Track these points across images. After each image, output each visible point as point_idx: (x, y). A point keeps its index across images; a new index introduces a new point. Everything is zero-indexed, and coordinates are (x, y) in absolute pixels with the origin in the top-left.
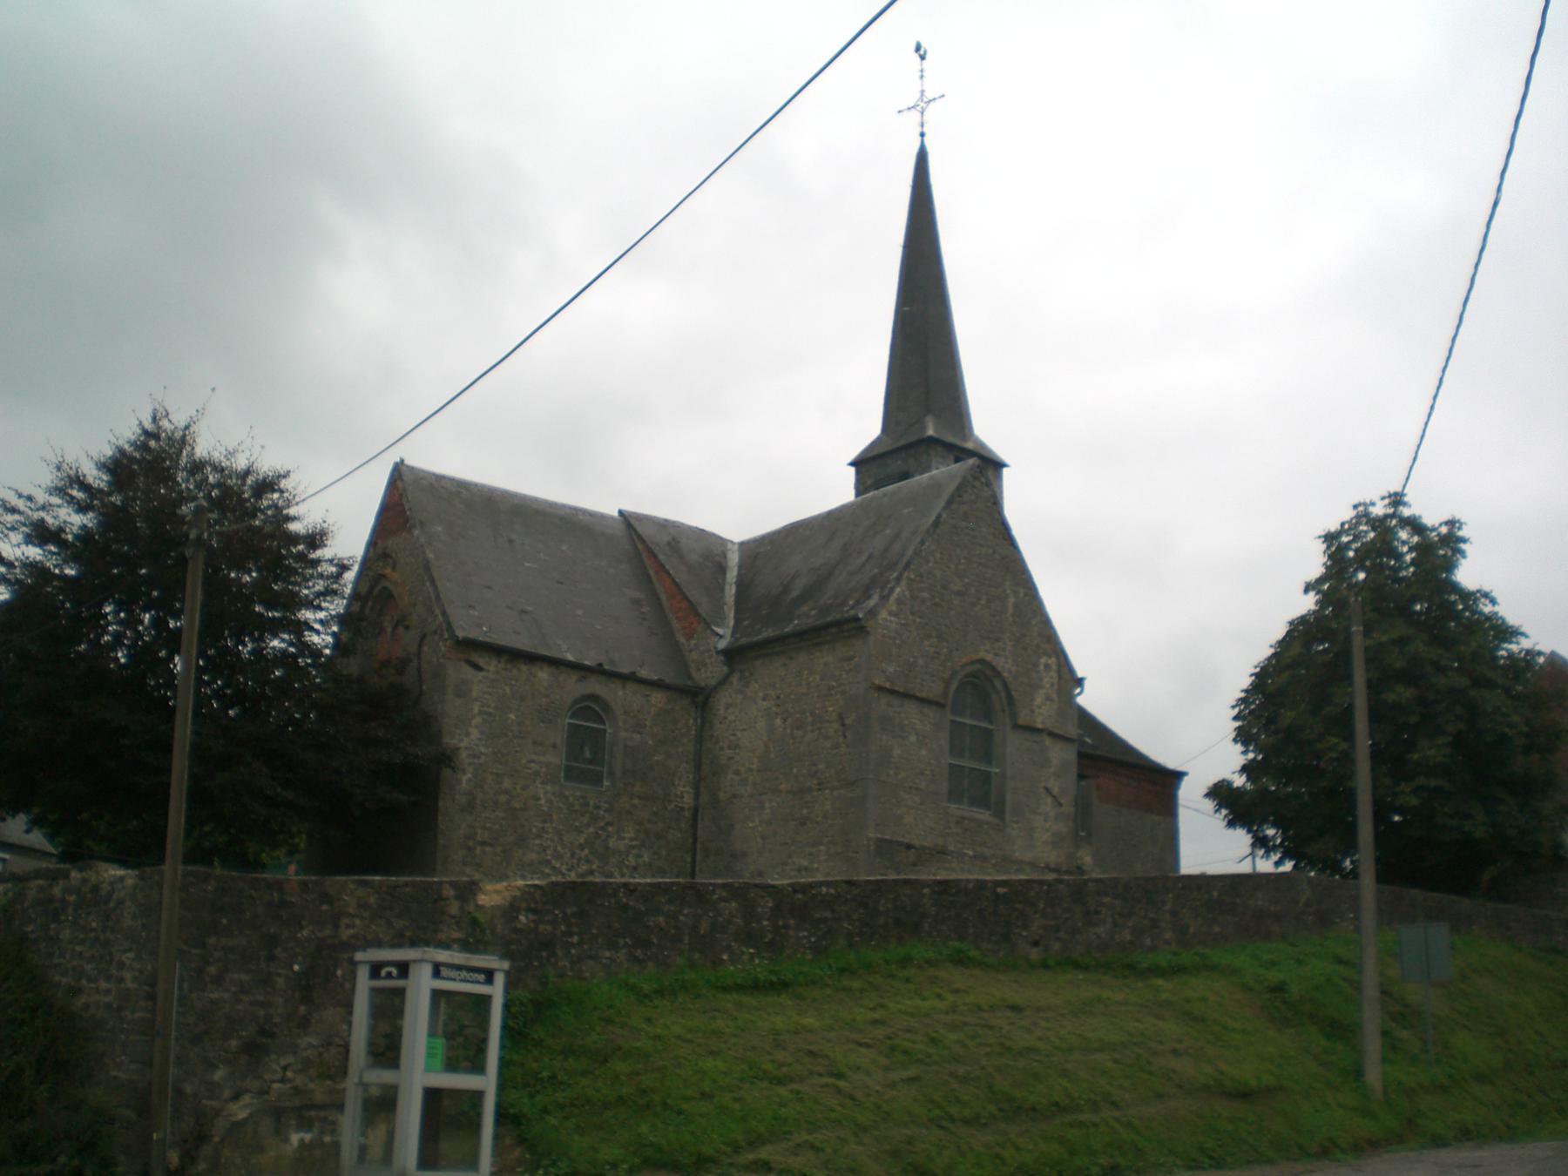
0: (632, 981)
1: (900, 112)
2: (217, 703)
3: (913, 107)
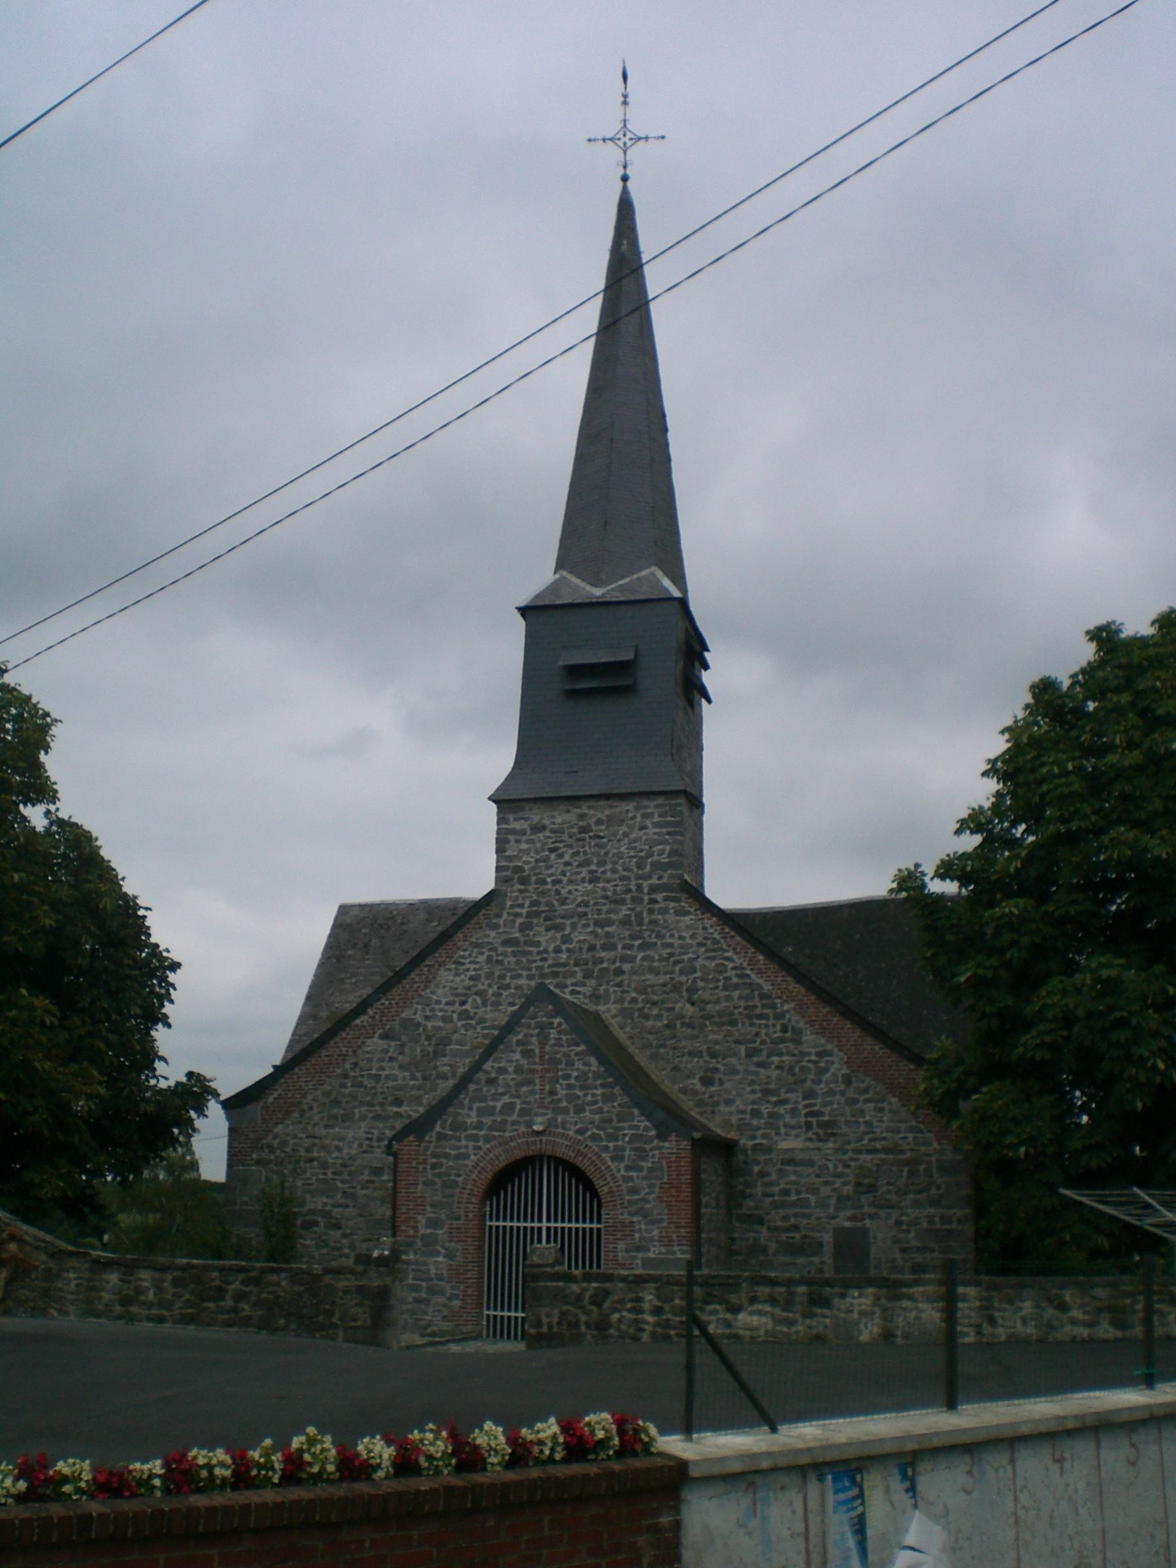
0: (370, 1012)
1: (590, 140)
2: (1135, 1150)
3: (611, 139)
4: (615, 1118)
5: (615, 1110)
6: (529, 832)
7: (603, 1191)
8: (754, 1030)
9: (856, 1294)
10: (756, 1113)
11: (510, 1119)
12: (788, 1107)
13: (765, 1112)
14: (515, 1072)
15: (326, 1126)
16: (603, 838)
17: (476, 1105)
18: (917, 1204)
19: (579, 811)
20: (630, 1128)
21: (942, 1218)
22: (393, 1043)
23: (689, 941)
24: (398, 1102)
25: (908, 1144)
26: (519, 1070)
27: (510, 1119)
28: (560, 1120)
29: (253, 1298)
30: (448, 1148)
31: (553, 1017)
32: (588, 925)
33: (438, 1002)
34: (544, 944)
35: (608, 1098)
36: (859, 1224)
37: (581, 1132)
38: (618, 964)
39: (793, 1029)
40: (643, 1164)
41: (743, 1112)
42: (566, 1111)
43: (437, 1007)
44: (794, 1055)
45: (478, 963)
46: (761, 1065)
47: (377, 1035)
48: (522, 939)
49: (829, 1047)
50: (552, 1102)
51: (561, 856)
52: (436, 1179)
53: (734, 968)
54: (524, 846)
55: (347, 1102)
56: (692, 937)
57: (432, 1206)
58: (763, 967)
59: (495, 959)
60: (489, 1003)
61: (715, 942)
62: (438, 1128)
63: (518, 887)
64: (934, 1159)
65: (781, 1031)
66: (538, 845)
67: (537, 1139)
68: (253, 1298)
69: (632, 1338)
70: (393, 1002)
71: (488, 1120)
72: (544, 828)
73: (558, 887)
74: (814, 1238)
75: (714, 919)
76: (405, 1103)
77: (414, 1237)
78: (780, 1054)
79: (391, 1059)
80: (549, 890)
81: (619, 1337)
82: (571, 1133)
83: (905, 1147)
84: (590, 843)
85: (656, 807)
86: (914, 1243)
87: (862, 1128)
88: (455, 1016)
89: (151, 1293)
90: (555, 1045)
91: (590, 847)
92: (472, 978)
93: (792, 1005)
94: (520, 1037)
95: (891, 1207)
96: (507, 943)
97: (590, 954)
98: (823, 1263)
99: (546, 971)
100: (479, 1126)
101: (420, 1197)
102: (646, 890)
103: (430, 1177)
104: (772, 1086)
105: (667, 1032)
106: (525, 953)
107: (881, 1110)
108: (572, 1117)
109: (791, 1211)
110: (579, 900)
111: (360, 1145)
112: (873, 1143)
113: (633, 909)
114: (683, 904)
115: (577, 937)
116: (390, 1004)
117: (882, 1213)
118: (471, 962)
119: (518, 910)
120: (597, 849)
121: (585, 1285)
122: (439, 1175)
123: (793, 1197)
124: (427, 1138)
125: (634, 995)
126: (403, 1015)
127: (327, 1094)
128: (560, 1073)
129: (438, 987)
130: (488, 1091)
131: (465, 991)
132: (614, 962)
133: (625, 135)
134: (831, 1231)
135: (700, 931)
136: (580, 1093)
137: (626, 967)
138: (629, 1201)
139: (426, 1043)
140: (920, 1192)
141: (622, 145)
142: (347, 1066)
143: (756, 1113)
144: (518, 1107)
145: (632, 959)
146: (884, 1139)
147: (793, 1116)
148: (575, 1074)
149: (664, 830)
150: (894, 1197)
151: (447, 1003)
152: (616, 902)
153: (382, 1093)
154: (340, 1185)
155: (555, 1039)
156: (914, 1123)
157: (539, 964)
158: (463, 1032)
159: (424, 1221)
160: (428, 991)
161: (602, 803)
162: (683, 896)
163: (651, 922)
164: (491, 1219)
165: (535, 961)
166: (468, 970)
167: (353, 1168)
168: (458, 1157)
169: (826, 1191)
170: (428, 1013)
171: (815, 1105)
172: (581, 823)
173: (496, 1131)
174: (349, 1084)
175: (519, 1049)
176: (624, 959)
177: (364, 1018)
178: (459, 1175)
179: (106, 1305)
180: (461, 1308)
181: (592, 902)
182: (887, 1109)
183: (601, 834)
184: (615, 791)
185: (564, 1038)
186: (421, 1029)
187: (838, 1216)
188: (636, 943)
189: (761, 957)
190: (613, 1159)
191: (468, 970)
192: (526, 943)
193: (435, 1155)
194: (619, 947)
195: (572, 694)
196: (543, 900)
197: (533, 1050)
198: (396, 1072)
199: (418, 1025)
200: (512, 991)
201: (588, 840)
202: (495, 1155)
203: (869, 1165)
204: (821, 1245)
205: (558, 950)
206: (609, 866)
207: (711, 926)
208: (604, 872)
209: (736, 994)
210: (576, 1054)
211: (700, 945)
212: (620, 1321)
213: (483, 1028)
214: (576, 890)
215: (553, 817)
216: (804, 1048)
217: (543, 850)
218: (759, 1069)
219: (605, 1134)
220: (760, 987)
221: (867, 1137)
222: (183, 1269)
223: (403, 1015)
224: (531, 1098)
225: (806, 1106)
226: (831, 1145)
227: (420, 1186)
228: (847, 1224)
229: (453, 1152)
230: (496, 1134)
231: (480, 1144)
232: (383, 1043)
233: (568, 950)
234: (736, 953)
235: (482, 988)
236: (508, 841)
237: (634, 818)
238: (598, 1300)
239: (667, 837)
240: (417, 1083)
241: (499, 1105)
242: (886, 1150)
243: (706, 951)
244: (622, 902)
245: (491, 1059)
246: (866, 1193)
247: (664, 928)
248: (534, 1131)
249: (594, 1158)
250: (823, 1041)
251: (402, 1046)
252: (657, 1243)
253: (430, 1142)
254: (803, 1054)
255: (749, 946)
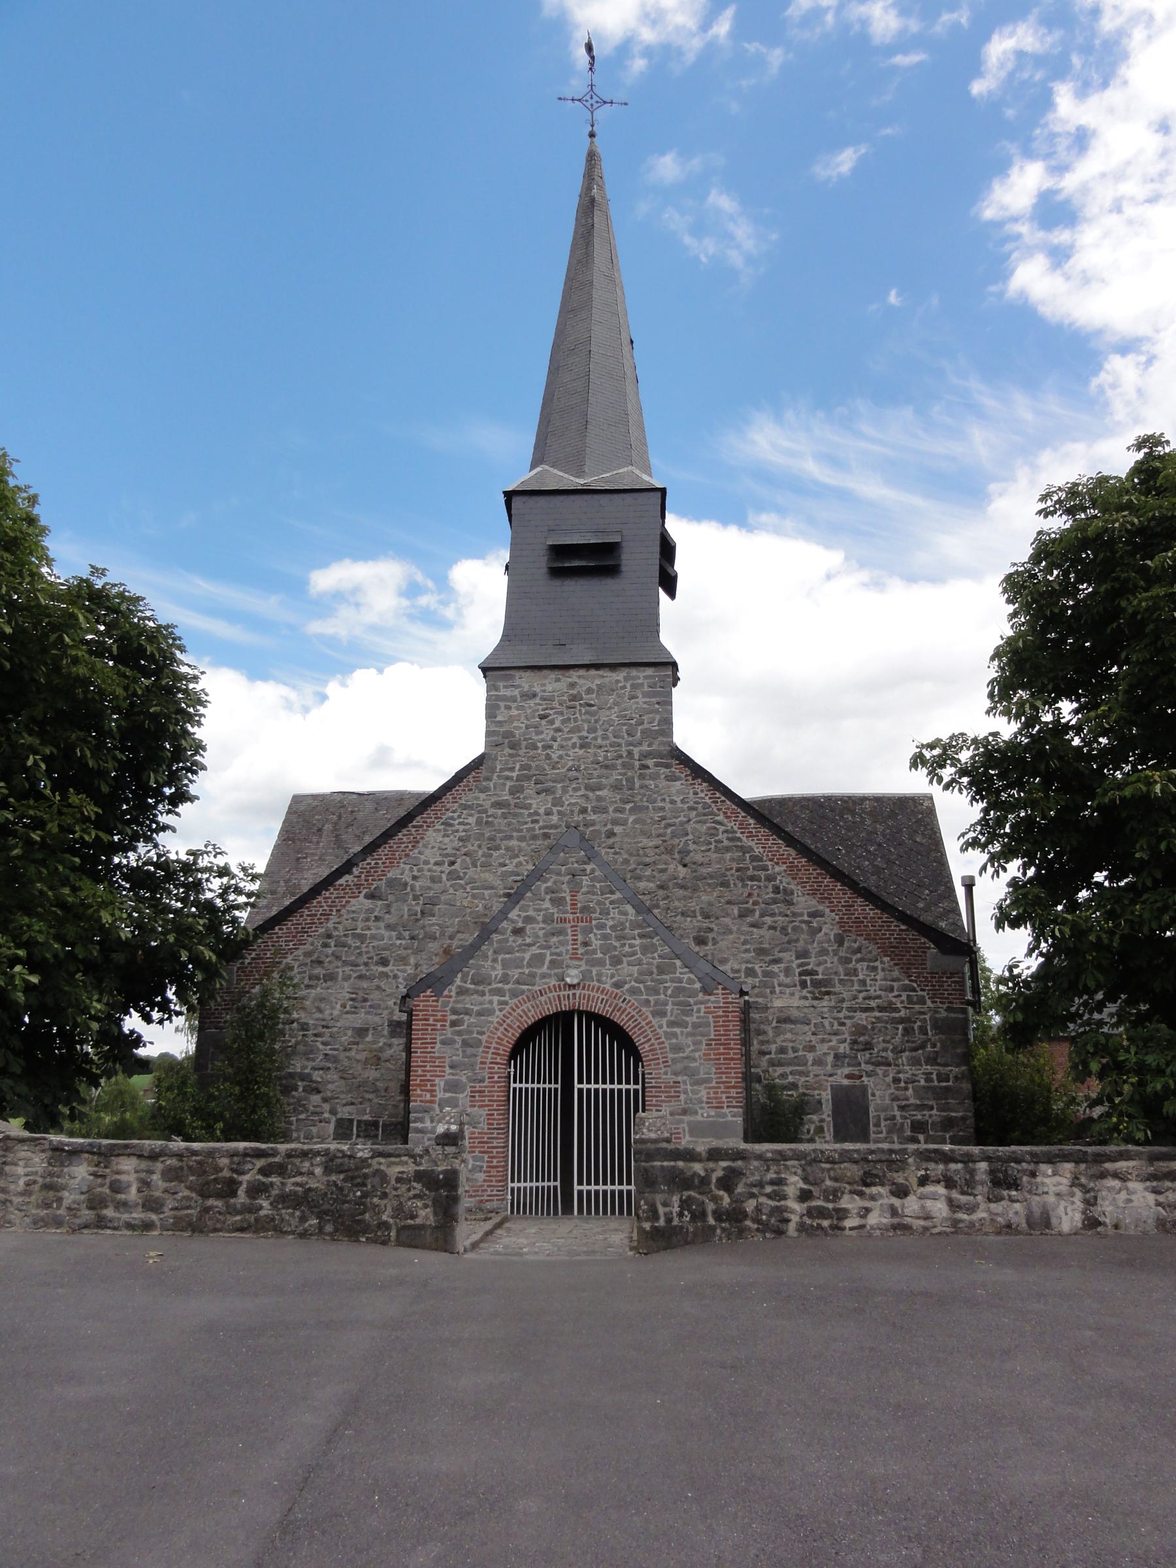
0: (356, 871)
4: (655, 971)
5: (655, 962)
6: (519, 700)
7: (644, 1049)
8: (747, 891)
9: (1050, 1172)
10: (750, 972)
11: (539, 971)
12: (782, 965)
13: (759, 971)
14: (544, 922)
15: (308, 987)
16: (592, 705)
17: (500, 958)
18: (915, 1062)
19: (569, 680)
20: (672, 981)
21: (939, 1075)
22: (380, 903)
23: (679, 805)
24: (384, 962)
25: (902, 1002)
26: (548, 919)
27: (539, 971)
28: (594, 973)
29: (275, 1192)
30: (468, 1002)
31: (585, 863)
32: (579, 789)
33: (426, 862)
34: (534, 806)
35: (645, 949)
36: (858, 1082)
37: (617, 985)
38: (609, 826)
39: (785, 890)
40: (687, 1019)
41: (738, 971)
42: (601, 963)
43: (426, 867)
44: (787, 916)
45: (468, 824)
46: (753, 925)
47: (362, 895)
48: (512, 802)
49: (821, 908)
50: (586, 953)
51: (552, 722)
52: (456, 1038)
53: (726, 831)
54: (515, 712)
55: (329, 962)
56: (683, 801)
57: (451, 1067)
58: (754, 831)
59: (485, 820)
60: (479, 864)
61: (706, 806)
62: (458, 981)
63: (507, 751)
64: (927, 1017)
65: (773, 892)
66: (529, 711)
67: (571, 993)
68: (275, 1192)
69: (774, 1232)
70: (380, 862)
71: (515, 973)
72: (534, 695)
73: (548, 751)
74: (813, 1096)
75: (705, 784)
76: (391, 963)
77: (432, 1102)
78: (773, 915)
79: (377, 919)
80: (539, 755)
81: (758, 1230)
82: (607, 986)
83: (899, 1005)
84: (580, 710)
85: (645, 677)
86: (912, 1101)
87: (856, 987)
88: (444, 876)
89: (134, 1190)
90: (588, 893)
91: (581, 715)
92: (461, 839)
93: (784, 867)
94: (549, 884)
95: (889, 1065)
96: (498, 805)
97: (581, 816)
98: (822, 1121)
99: (537, 832)
100: (505, 979)
101: (439, 1058)
102: (636, 757)
103: (449, 1035)
104: (766, 946)
105: (661, 893)
106: (515, 815)
107: (874, 969)
108: (608, 970)
109: (788, 1069)
110: (570, 764)
111: (344, 1006)
112: (867, 1002)
113: (625, 774)
114: (673, 770)
115: (569, 799)
116: (376, 863)
117: (880, 1070)
118: (460, 824)
119: (507, 773)
120: (588, 717)
121: (711, 1165)
122: (459, 1033)
123: (791, 1055)
124: (446, 993)
125: (626, 856)
126: (389, 875)
127: (308, 954)
128: (594, 922)
129: (427, 847)
130: (514, 941)
131: (454, 852)
132: (605, 825)
133: (592, 98)
134: (829, 1088)
135: (691, 795)
136: (617, 944)
137: (618, 829)
138: (673, 1060)
139: (414, 903)
140: (915, 1049)
141: (594, 97)
142: (330, 925)
143: (750, 972)
144: (548, 958)
145: (624, 823)
146: (879, 997)
147: (787, 976)
148: (611, 923)
149: (654, 700)
150: (890, 1055)
151: (436, 864)
152: (607, 767)
153: (367, 953)
154: (321, 1047)
155: (588, 886)
156: (907, 982)
157: (530, 825)
158: (451, 891)
159: (442, 1084)
160: (416, 851)
161: (593, 672)
162: (674, 762)
163: (642, 787)
164: (515, 1082)
165: (526, 823)
166: (457, 831)
167: (335, 1029)
168: (480, 1014)
169: (822, 1049)
170: (415, 873)
171: (808, 964)
172: (571, 692)
173: (525, 984)
174: (333, 944)
175: (548, 897)
176: (615, 822)
177: (347, 877)
178: (483, 1033)
179: (69, 1209)
180: (485, 1181)
181: (583, 767)
182: (880, 968)
183: (592, 702)
184: (605, 662)
185: (598, 885)
186: (409, 889)
187: (836, 1074)
188: (628, 806)
189: (752, 821)
190: (654, 1014)
191: (457, 831)
192: (516, 806)
193: (454, 1012)
194: (611, 809)
195: (557, 573)
196: (533, 764)
197: (564, 898)
198: (383, 931)
199: (406, 884)
200: (503, 852)
201: (578, 708)
202: (523, 1011)
203: (864, 1023)
204: (819, 1102)
205: (548, 813)
206: (600, 733)
207: (702, 791)
208: (595, 739)
209: (728, 856)
210: (612, 903)
211: (691, 809)
212: (758, 1209)
213: (473, 889)
214: (567, 755)
215: (544, 685)
216: (797, 909)
217: (534, 717)
218: (752, 929)
219: (645, 987)
220: (751, 849)
221: (861, 995)
222: (179, 1156)
223: (389, 875)
224: (562, 949)
225: (799, 966)
226: (825, 1003)
227: (438, 1046)
228: (846, 1082)
229: (476, 1008)
230: (525, 987)
231: (507, 998)
232: (368, 903)
233: (559, 813)
234: (727, 817)
235: (472, 848)
236: (498, 707)
237: (624, 687)
238: (727, 1183)
239: (657, 706)
240: (403, 942)
241: (527, 956)
242: (881, 1009)
243: (697, 815)
244: (613, 767)
245: (517, 908)
246: (864, 1050)
247: (654, 793)
248: (566, 984)
249: (634, 1013)
250: (814, 902)
251: (388, 906)
252: (704, 1105)
253: (450, 997)
254: (794, 914)
255: (739, 810)
